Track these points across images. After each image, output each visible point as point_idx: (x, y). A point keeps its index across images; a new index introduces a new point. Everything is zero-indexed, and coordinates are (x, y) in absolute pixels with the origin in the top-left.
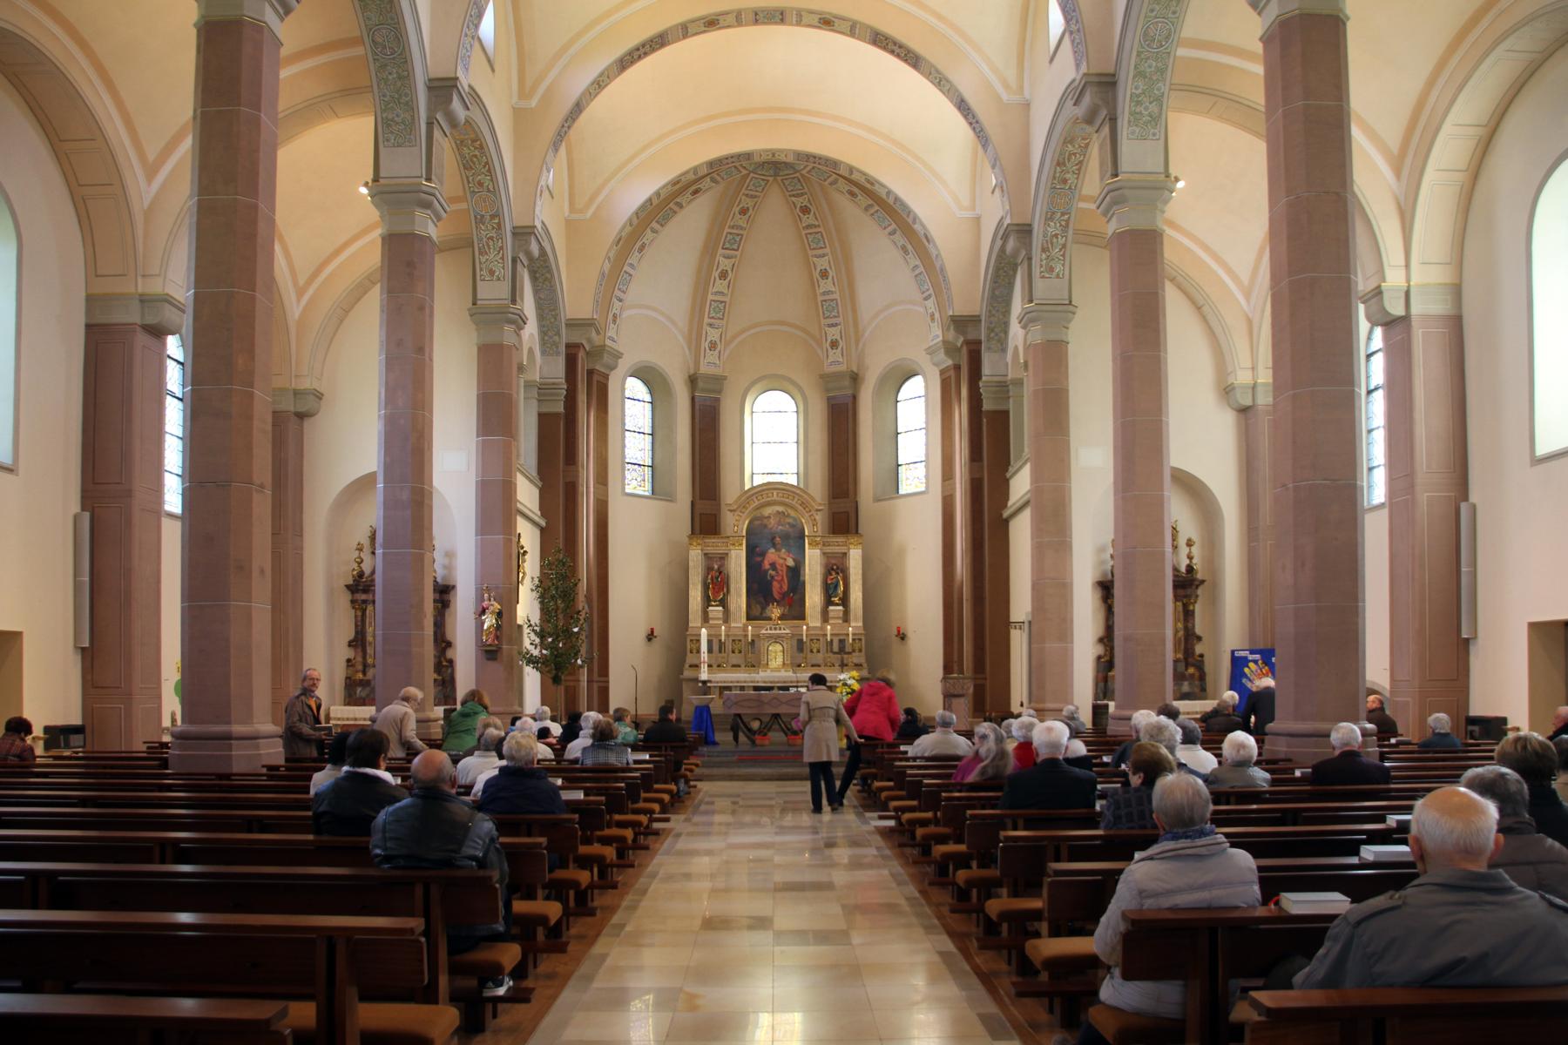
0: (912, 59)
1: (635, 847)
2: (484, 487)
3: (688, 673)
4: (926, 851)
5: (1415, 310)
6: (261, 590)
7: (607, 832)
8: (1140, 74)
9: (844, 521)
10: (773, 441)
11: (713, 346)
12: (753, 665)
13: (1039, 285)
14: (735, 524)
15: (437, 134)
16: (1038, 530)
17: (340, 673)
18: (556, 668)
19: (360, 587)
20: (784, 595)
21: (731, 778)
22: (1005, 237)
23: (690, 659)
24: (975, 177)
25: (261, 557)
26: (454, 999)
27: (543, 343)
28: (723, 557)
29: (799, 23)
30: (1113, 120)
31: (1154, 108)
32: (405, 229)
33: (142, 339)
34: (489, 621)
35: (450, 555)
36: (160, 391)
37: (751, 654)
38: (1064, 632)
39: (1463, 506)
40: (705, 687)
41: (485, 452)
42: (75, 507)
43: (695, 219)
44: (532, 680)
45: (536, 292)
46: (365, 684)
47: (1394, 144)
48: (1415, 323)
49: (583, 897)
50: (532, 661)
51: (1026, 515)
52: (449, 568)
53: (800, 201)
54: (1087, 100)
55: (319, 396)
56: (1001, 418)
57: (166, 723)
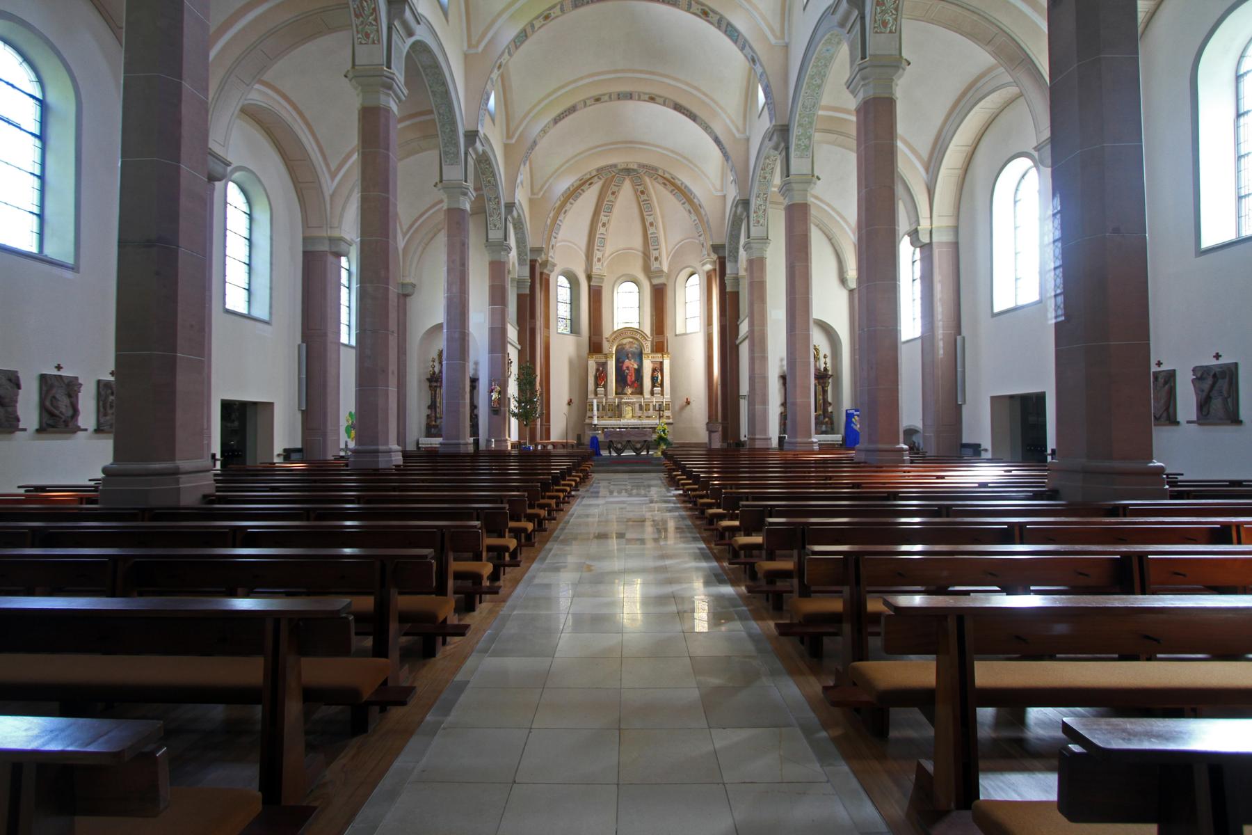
0: (693, 117)
1: (564, 501)
2: (492, 330)
3: (587, 421)
5: (935, 239)
6: (393, 381)
7: (542, 501)
8: (800, 125)
9: (659, 348)
10: (627, 308)
11: (599, 260)
12: (620, 416)
13: (752, 229)
14: (610, 348)
15: (395, 37)
16: (752, 350)
17: (424, 421)
18: (525, 416)
19: (434, 380)
20: (633, 383)
22: (736, 206)
23: (589, 414)
24: (723, 175)
25: (393, 367)
26: (489, 560)
27: (519, 259)
28: (604, 365)
29: (639, 99)
30: (787, 148)
31: (807, 142)
32: (456, 206)
33: (331, 258)
34: (495, 396)
35: (476, 363)
36: (339, 284)
37: (617, 411)
38: (765, 402)
39: (959, 338)
40: (595, 428)
41: (493, 313)
42: (299, 340)
43: (590, 196)
44: (514, 422)
45: (516, 234)
46: (436, 427)
47: (925, 156)
48: (934, 246)
49: (529, 537)
50: (515, 415)
51: (746, 342)
52: (476, 370)
53: (640, 188)
54: (775, 138)
55: (414, 286)
56: (736, 295)
57: (342, 446)
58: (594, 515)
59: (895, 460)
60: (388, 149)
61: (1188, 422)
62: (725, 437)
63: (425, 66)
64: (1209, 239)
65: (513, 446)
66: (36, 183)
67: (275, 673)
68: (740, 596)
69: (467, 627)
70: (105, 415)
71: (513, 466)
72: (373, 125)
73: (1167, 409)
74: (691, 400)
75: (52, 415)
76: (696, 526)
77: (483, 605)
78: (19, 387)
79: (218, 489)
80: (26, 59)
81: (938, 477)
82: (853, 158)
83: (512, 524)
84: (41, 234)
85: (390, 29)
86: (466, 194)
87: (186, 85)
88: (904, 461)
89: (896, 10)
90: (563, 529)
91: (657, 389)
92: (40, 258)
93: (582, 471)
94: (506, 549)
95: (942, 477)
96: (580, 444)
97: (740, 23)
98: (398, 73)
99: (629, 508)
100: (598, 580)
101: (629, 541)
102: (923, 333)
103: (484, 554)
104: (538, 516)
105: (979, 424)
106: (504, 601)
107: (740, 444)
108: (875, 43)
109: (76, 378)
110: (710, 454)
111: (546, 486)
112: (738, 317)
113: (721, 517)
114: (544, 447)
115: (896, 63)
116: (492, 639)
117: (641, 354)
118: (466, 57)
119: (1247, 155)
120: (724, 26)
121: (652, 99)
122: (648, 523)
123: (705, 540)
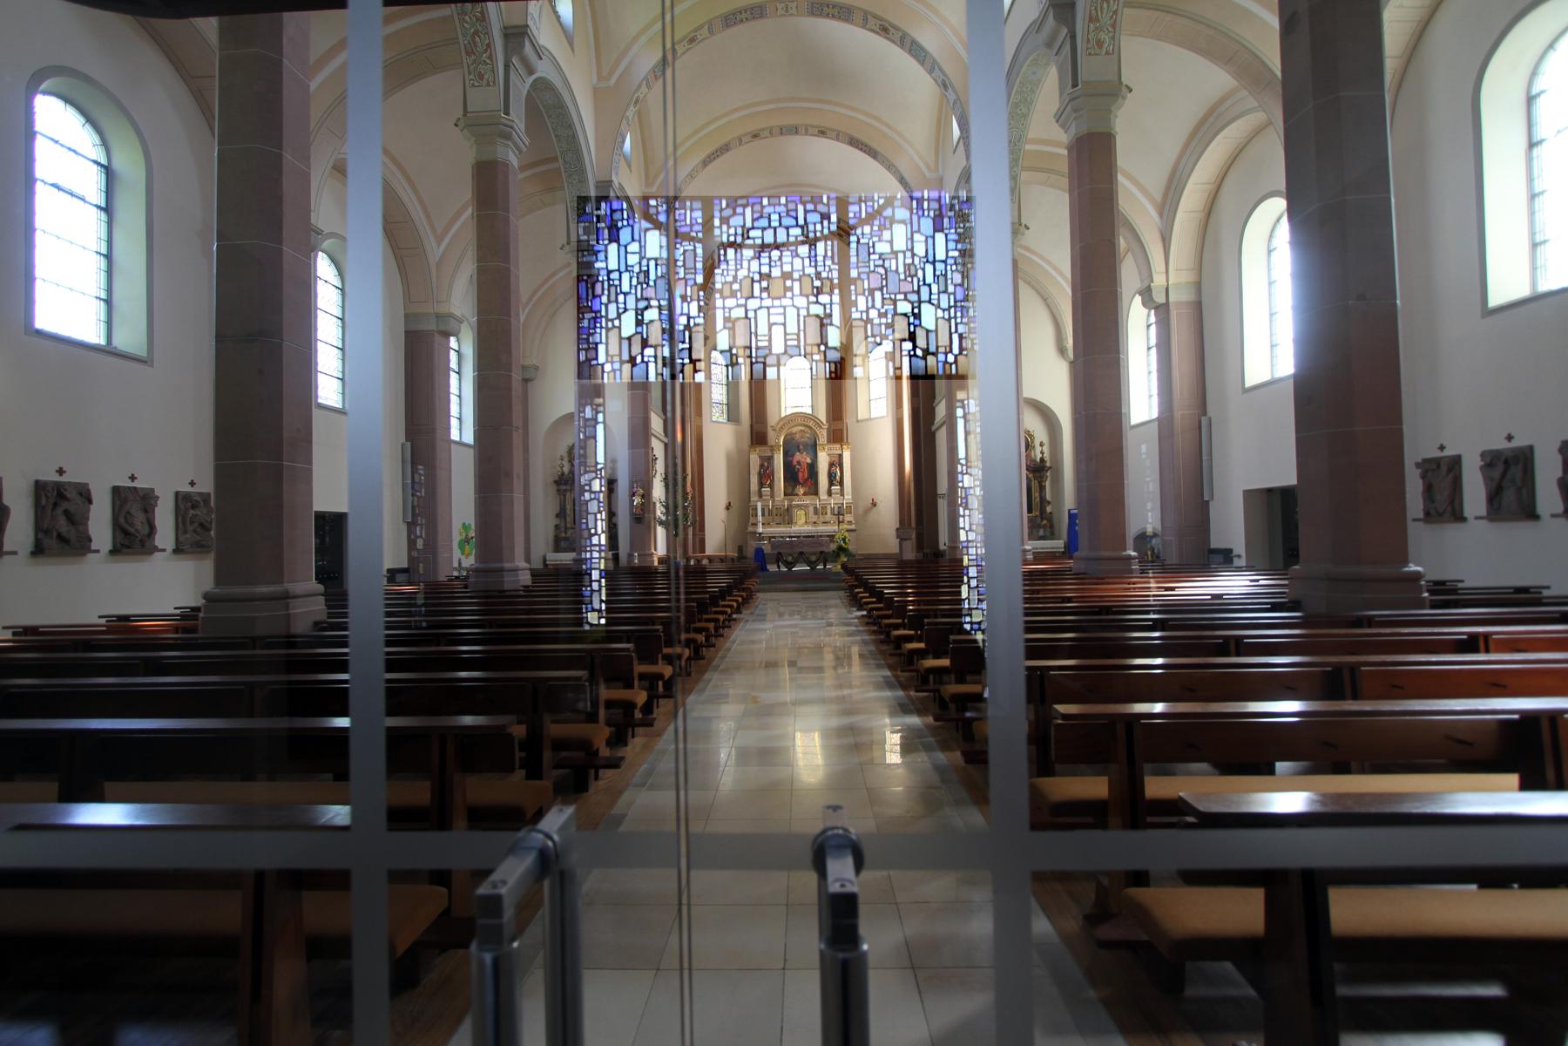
3: (750, 529)
4: (898, 647)
5: (1171, 299)
7: (698, 625)
9: (837, 436)
15: (513, 76)
18: (672, 526)
20: (805, 481)
21: (776, 590)
23: (752, 520)
26: (608, 724)
28: (770, 459)
36: (449, 369)
37: (786, 516)
40: (760, 537)
44: (661, 532)
46: (566, 539)
47: (1158, 197)
49: (669, 685)
50: (661, 523)
51: (944, 429)
55: (537, 368)
57: (456, 565)
58: (760, 641)
59: (1121, 569)
60: (507, 210)
61: (1553, 516)
62: (920, 546)
63: (548, 108)
64: (1496, 298)
65: (661, 561)
66: (103, 263)
67: (443, 792)
68: (928, 726)
69: (622, 758)
70: (185, 532)
71: (660, 584)
72: (489, 184)
73: (1452, 502)
74: (877, 500)
75: (126, 533)
76: (881, 652)
77: (637, 740)
78: (90, 502)
79: (330, 615)
80: (90, 119)
81: (1167, 589)
82: (1065, 198)
83: (666, 650)
84: (109, 323)
85: (507, 67)
86: (508, 137)
87: (287, 156)
88: (1131, 571)
89: (1113, 26)
90: (723, 657)
91: (836, 488)
92: (108, 351)
93: (744, 590)
94: (661, 676)
95: (1173, 589)
96: (742, 557)
97: (927, 40)
98: (518, 118)
99: (801, 633)
100: (765, 712)
101: (801, 670)
102: (1160, 412)
103: (636, 683)
104: (694, 641)
105: (1230, 525)
106: (660, 735)
107: (938, 554)
108: (1089, 68)
109: (152, 490)
110: (902, 566)
111: (703, 607)
112: (933, 397)
113: (922, 654)
114: (698, 561)
115: (1113, 91)
116: (649, 773)
117: (815, 446)
118: (596, 92)
119: (1542, 193)
120: (908, 44)
121: (822, 133)
122: (827, 649)
123: (890, 667)
